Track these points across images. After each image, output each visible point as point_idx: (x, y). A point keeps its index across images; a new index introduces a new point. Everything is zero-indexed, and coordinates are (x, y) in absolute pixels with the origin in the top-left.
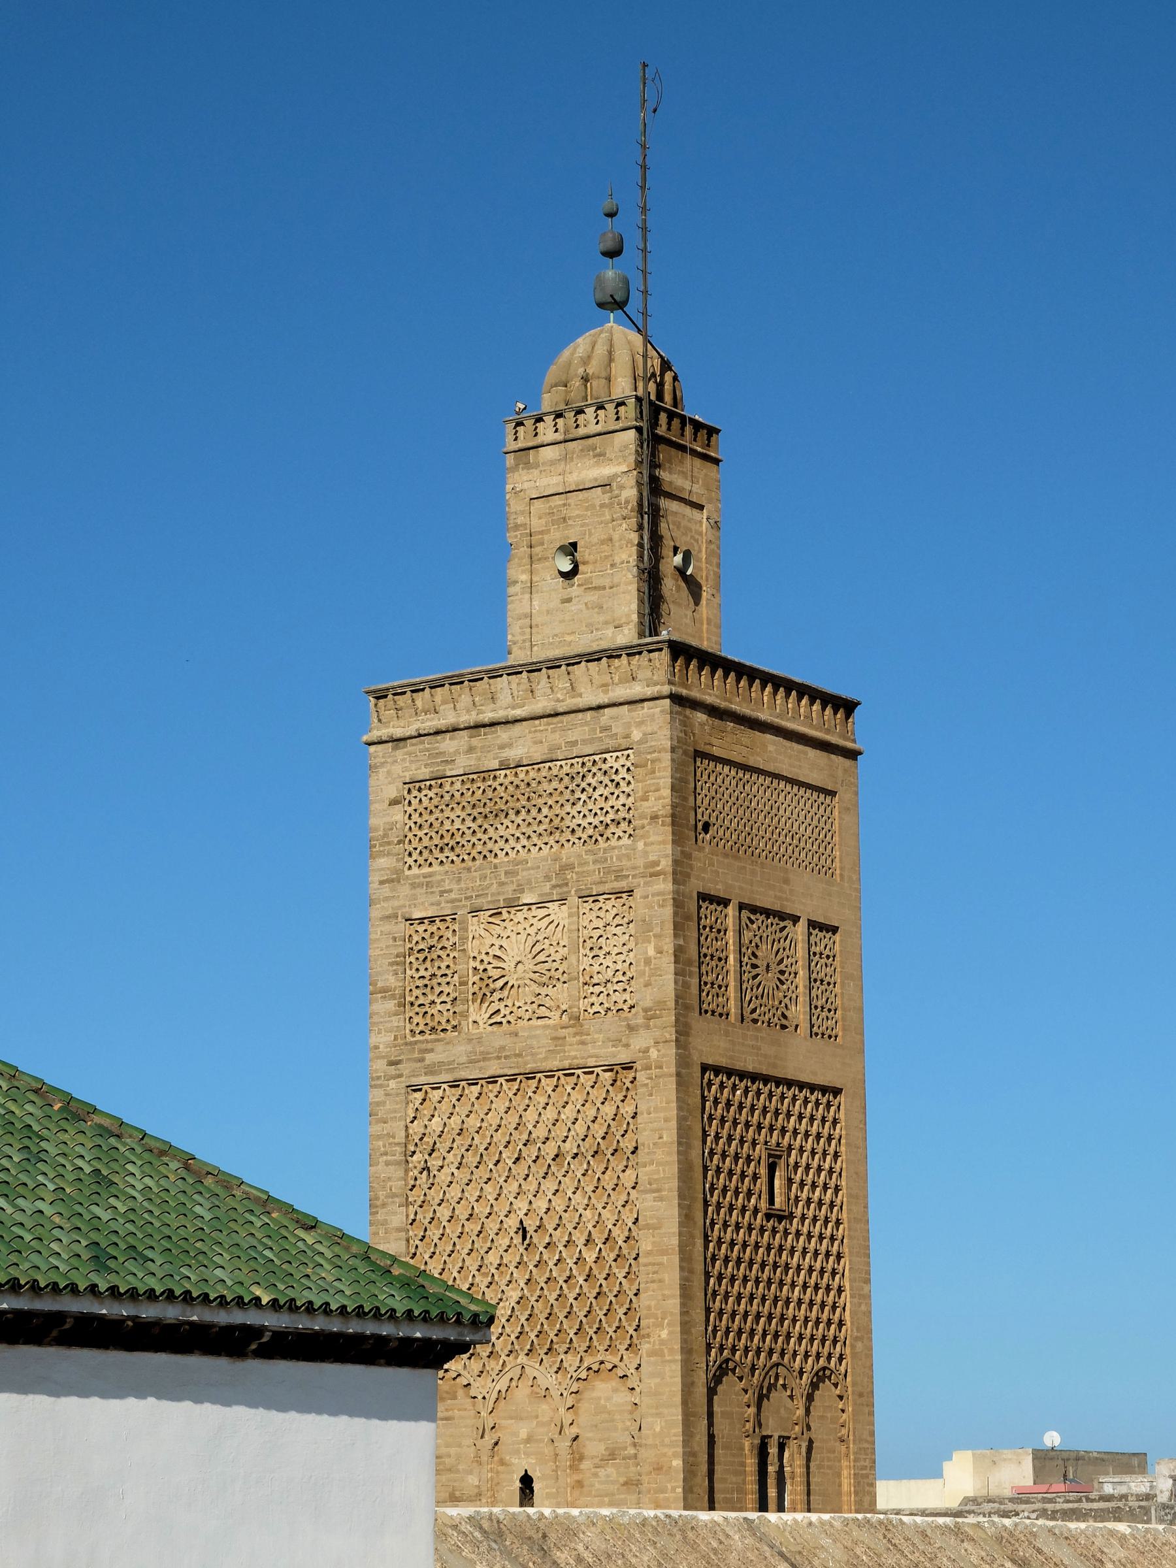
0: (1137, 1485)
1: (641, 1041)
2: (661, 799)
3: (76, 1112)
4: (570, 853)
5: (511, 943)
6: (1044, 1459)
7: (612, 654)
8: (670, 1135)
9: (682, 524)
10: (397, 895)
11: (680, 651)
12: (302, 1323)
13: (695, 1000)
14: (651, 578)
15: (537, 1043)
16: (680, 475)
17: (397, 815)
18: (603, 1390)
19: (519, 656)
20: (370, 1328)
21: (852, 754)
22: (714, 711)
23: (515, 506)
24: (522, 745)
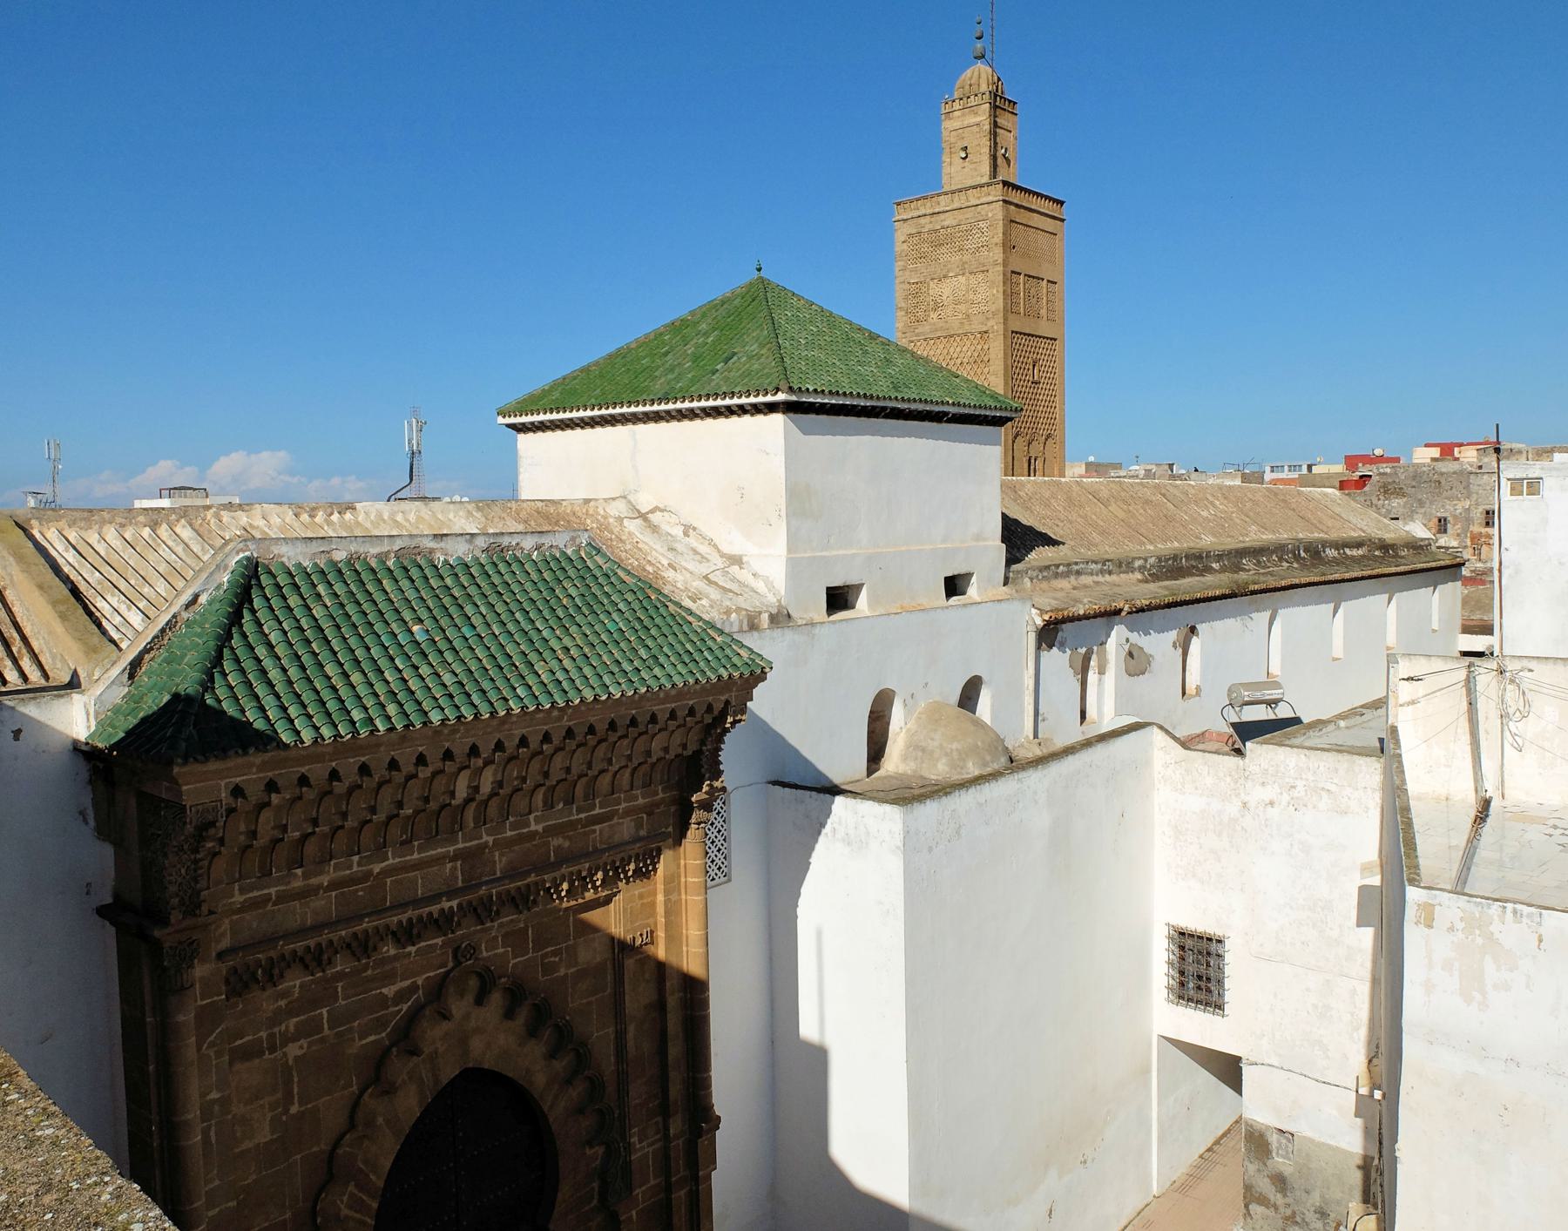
1: (990, 323)
2: (999, 238)
3: (873, 337)
4: (966, 258)
5: (945, 290)
6: (1088, 465)
7: (982, 186)
8: (1001, 355)
9: (1005, 138)
10: (903, 275)
11: (1005, 183)
13: (1010, 309)
14: (994, 158)
17: (905, 246)
20: (983, 412)
22: (1017, 206)
23: (945, 133)
24: (949, 220)
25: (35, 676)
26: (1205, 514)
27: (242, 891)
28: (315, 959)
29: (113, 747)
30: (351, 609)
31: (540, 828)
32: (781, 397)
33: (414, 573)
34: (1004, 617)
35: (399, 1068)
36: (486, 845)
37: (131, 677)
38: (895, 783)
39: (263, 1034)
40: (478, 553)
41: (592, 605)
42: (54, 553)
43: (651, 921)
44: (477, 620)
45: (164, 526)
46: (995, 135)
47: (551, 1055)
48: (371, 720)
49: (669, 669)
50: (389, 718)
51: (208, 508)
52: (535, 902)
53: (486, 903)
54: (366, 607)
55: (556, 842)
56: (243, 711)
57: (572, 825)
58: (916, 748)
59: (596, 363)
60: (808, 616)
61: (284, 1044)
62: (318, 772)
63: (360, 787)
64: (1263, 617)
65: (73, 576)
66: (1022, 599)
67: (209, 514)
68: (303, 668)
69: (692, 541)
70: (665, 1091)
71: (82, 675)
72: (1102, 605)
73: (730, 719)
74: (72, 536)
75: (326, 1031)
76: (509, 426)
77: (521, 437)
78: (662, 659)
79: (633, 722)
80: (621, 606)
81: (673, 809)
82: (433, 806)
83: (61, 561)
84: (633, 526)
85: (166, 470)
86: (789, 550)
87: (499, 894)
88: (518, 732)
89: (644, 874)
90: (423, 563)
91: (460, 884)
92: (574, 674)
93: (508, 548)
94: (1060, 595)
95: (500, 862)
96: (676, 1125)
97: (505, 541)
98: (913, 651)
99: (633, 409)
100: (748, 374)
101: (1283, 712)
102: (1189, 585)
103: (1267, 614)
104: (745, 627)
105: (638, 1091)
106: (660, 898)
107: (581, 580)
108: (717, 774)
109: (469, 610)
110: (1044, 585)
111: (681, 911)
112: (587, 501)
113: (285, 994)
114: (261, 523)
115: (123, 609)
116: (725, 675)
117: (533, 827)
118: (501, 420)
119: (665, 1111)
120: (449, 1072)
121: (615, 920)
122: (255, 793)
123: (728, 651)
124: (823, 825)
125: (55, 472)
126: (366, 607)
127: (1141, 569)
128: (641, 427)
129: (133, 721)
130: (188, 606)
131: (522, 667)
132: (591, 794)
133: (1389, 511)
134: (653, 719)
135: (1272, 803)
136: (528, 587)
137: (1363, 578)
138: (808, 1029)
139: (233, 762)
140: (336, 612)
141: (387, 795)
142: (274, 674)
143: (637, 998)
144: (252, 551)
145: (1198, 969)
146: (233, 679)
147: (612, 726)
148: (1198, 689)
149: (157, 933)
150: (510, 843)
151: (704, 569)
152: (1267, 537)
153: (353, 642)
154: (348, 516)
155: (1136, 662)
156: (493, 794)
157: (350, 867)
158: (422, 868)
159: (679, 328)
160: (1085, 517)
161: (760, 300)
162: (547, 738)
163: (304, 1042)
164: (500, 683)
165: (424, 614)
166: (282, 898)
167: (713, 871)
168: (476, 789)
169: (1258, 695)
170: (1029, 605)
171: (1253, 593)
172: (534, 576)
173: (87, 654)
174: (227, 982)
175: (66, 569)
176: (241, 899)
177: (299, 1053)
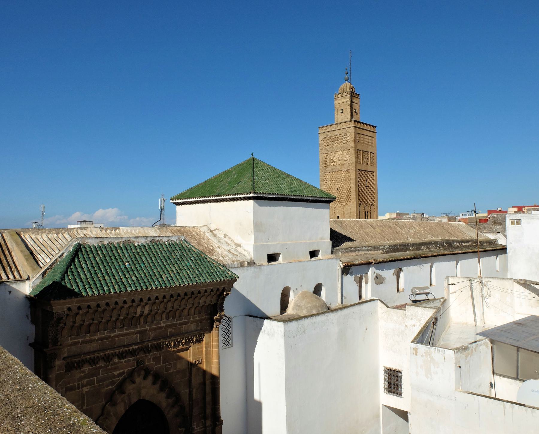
0: (408, 216)
2: (353, 139)
3: (288, 175)
5: (335, 156)
6: (397, 214)
8: (354, 177)
10: (322, 151)
11: (355, 121)
12: (314, 199)
13: (357, 162)
14: (352, 113)
15: (339, 167)
16: (355, 100)
18: (346, 206)
19: (336, 123)
21: (376, 133)
22: (359, 128)
23: (335, 105)
24: (337, 133)
25: (18, 277)
26: (411, 231)
27: (71, 339)
28: (93, 362)
29: (35, 296)
30: (107, 258)
31: (164, 325)
32: (251, 195)
33: (128, 248)
34: (330, 265)
35: (119, 398)
36: (146, 330)
37: (43, 276)
38: (289, 317)
39: (76, 384)
40: (148, 242)
41: (183, 258)
42: (27, 242)
43: (201, 356)
44: (145, 262)
45: (61, 234)
46: (352, 105)
47: (168, 397)
48: (109, 290)
49: (205, 277)
50: (115, 289)
51: (74, 228)
52: (163, 348)
53: (147, 347)
54: (112, 258)
55: (170, 330)
56: (72, 286)
57: (175, 325)
58: (297, 306)
59: (201, 184)
60: (261, 263)
61: (82, 387)
62: (93, 304)
63: (106, 309)
64: (427, 266)
65: (32, 248)
66: (336, 259)
67: (74, 230)
68: (91, 274)
69: (226, 239)
70: (205, 413)
71: (31, 276)
72: (366, 260)
73: (225, 293)
74: (33, 237)
75: (96, 384)
76: (174, 203)
77: (177, 206)
78: (203, 274)
79: (193, 293)
80: (192, 258)
81: (209, 321)
82: (130, 316)
83: (28, 244)
84: (208, 235)
85: (77, 215)
86: (255, 243)
87: (151, 345)
88: (155, 295)
89: (199, 341)
90: (131, 245)
91: (139, 341)
92: (174, 278)
93: (158, 241)
94: (350, 257)
95: (152, 335)
96: (208, 423)
97: (157, 239)
98: (297, 274)
99: (209, 198)
100: (243, 188)
101: (430, 297)
102: (399, 255)
103: (429, 265)
104: (239, 266)
105: (196, 411)
106: (204, 349)
107: (183, 251)
108: (222, 310)
109: (144, 259)
110: (346, 254)
111: (211, 353)
112: (194, 227)
113: (83, 372)
114: (90, 233)
115: (45, 258)
116: (222, 279)
117: (162, 325)
118: (171, 201)
119: (205, 418)
120: (134, 400)
121: (189, 356)
122: (75, 310)
123: (225, 273)
124: (261, 329)
125: (43, 215)
126: (112, 258)
127: (382, 249)
128: (212, 204)
129: (42, 289)
130: (60, 257)
131: (158, 276)
132: (181, 315)
133: (496, 230)
134: (199, 292)
135: (414, 326)
136: (163, 252)
137: (466, 253)
138: (257, 397)
139: (69, 300)
140: (103, 259)
141: (115, 313)
142: (83, 276)
143: (196, 381)
144: (80, 241)
145: (394, 382)
146: (70, 277)
147: (186, 294)
148: (403, 289)
149: (45, 350)
150: (155, 329)
151: (229, 248)
152: (434, 239)
153: (107, 267)
154: (117, 231)
155: (379, 280)
156: (149, 314)
157: (104, 334)
158: (128, 336)
159: (227, 173)
160: (366, 232)
161: (253, 163)
162: (164, 297)
163: (88, 387)
164: (150, 280)
165: (129, 260)
166: (83, 342)
167: (226, 343)
168: (143, 312)
169: (421, 291)
170: (339, 260)
171: (422, 257)
172: (165, 249)
173: (32, 271)
174: (66, 367)
175: (30, 246)
176: (71, 342)
177: (87, 390)
